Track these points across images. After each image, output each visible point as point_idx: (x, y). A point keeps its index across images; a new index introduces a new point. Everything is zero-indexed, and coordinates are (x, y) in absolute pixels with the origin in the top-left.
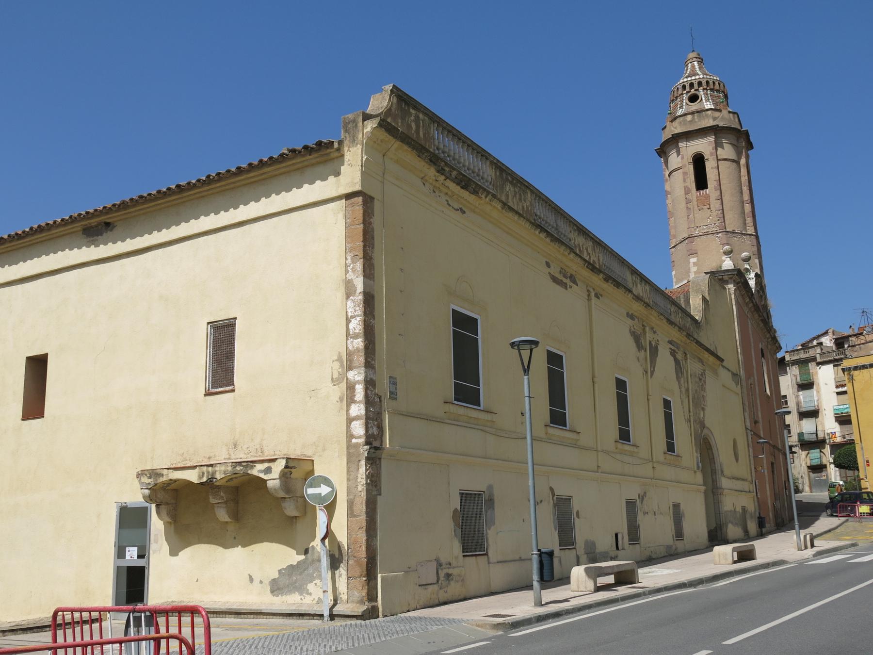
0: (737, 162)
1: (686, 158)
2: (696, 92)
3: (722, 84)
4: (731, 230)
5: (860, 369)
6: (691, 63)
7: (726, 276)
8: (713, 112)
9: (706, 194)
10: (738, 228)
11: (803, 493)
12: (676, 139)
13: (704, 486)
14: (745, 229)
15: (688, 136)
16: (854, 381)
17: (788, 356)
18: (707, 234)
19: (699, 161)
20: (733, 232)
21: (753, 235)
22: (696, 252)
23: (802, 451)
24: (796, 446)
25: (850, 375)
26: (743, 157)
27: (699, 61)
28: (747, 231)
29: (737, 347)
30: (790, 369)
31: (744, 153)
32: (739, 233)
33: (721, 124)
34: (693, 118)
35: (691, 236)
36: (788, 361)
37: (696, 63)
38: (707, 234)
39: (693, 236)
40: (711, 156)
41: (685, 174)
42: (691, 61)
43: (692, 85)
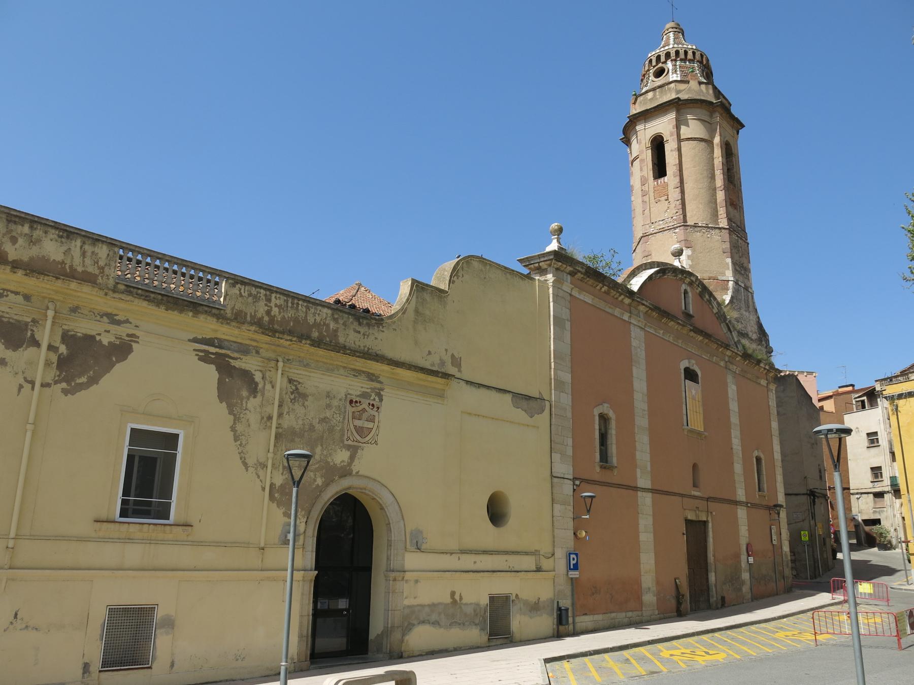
0: (709, 142)
1: (643, 142)
2: (663, 65)
3: (704, 57)
4: (693, 224)
5: (905, 397)
6: (666, 34)
7: (543, 263)
8: (676, 84)
9: (664, 182)
10: (702, 221)
11: (897, 549)
12: (634, 120)
13: (315, 570)
14: (716, 222)
15: (646, 115)
16: (899, 413)
17: (879, 385)
18: (662, 230)
19: (658, 145)
20: (695, 226)
21: (724, 229)
22: (650, 253)
23: (896, 498)
24: (888, 492)
25: (894, 405)
26: (716, 135)
27: (675, 32)
28: (718, 225)
29: (550, 360)
30: (880, 401)
31: (718, 130)
32: (705, 227)
33: (684, 96)
34: (655, 95)
35: (646, 235)
36: (878, 391)
37: (671, 35)
38: (662, 230)
39: (647, 234)
40: (671, 136)
41: (642, 161)
42: (666, 32)
43: (658, 58)
